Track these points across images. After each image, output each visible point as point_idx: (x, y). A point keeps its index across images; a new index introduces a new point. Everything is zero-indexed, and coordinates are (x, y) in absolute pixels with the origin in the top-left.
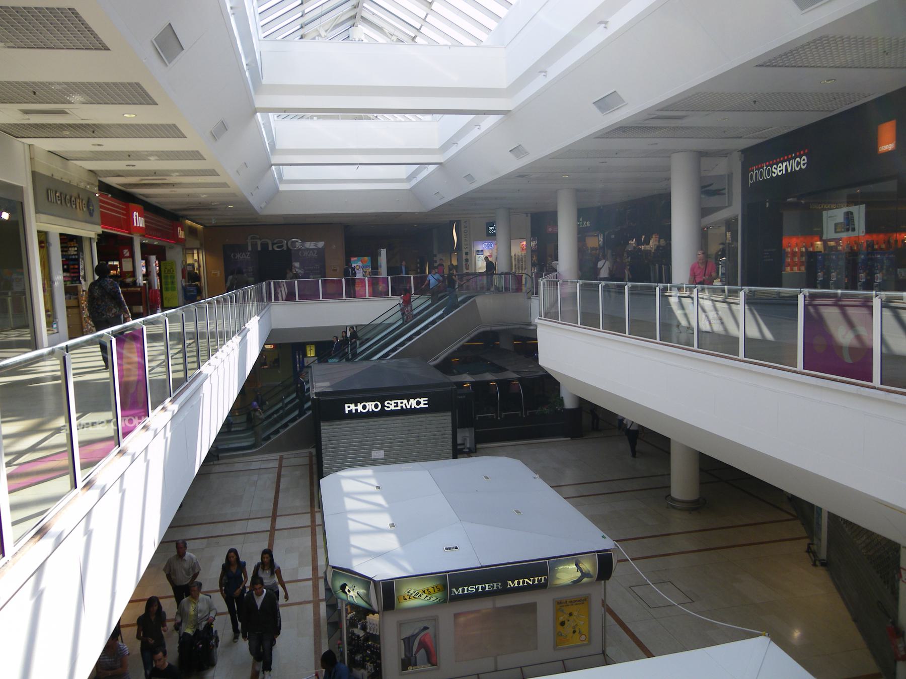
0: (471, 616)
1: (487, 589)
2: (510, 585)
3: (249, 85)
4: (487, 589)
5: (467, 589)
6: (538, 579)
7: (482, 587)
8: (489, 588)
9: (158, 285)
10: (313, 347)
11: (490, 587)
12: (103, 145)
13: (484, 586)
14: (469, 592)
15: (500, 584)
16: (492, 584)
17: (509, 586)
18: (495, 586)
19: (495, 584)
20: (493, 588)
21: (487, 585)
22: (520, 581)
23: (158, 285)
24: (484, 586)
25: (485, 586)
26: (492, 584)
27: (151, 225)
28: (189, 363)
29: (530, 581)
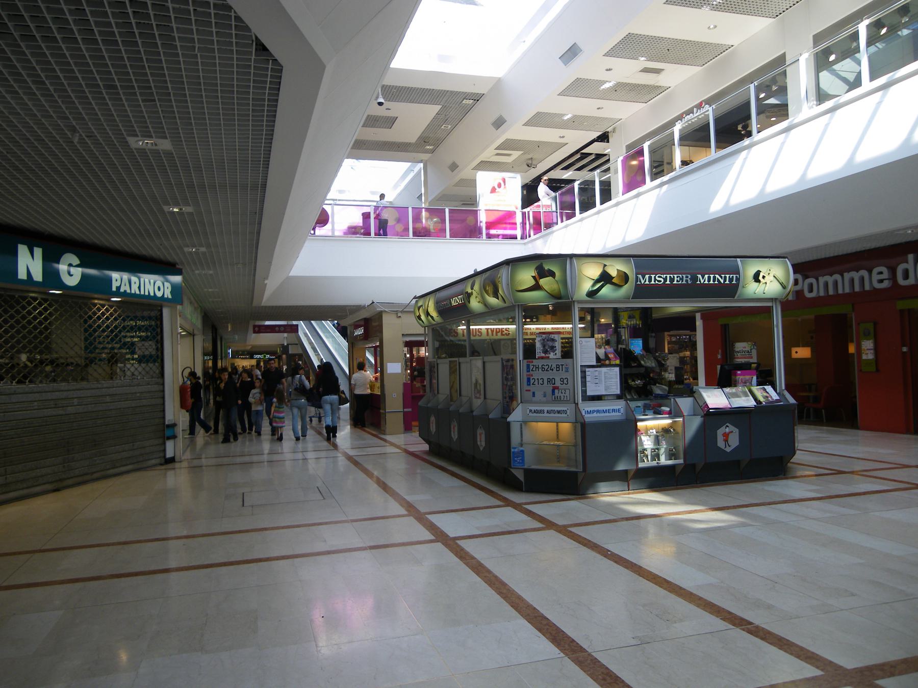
0: (828, 515)
1: (675, 282)
2: (700, 281)
3: (320, 328)
4: (675, 282)
5: (655, 277)
6: (729, 277)
7: (670, 277)
8: (677, 281)
9: (454, 432)
10: (794, 350)
11: (678, 279)
12: (612, 70)
13: (672, 276)
14: (657, 282)
15: (689, 276)
16: (681, 276)
17: (698, 282)
18: (684, 279)
19: (684, 276)
20: (682, 281)
21: (675, 276)
22: (713, 281)
23: (454, 432)
24: (672, 276)
25: (674, 277)
26: (681, 276)
27: (75, 224)
28: (499, 361)
29: (721, 277)
